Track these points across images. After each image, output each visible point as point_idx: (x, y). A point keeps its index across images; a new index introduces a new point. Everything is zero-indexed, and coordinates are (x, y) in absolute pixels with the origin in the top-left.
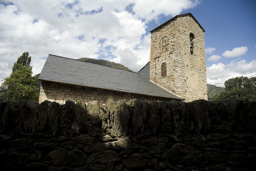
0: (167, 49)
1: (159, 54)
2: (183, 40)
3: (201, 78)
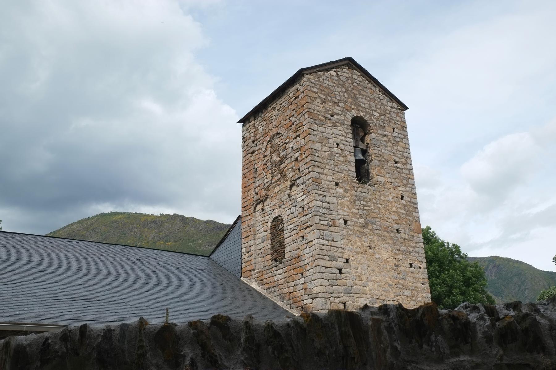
0: (282, 173)
1: (265, 189)
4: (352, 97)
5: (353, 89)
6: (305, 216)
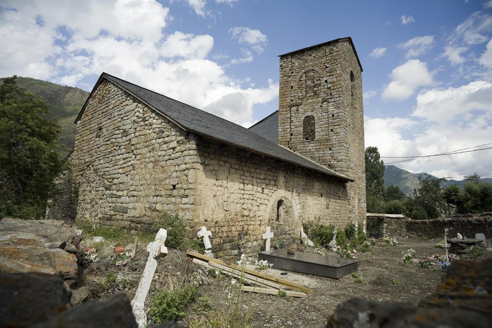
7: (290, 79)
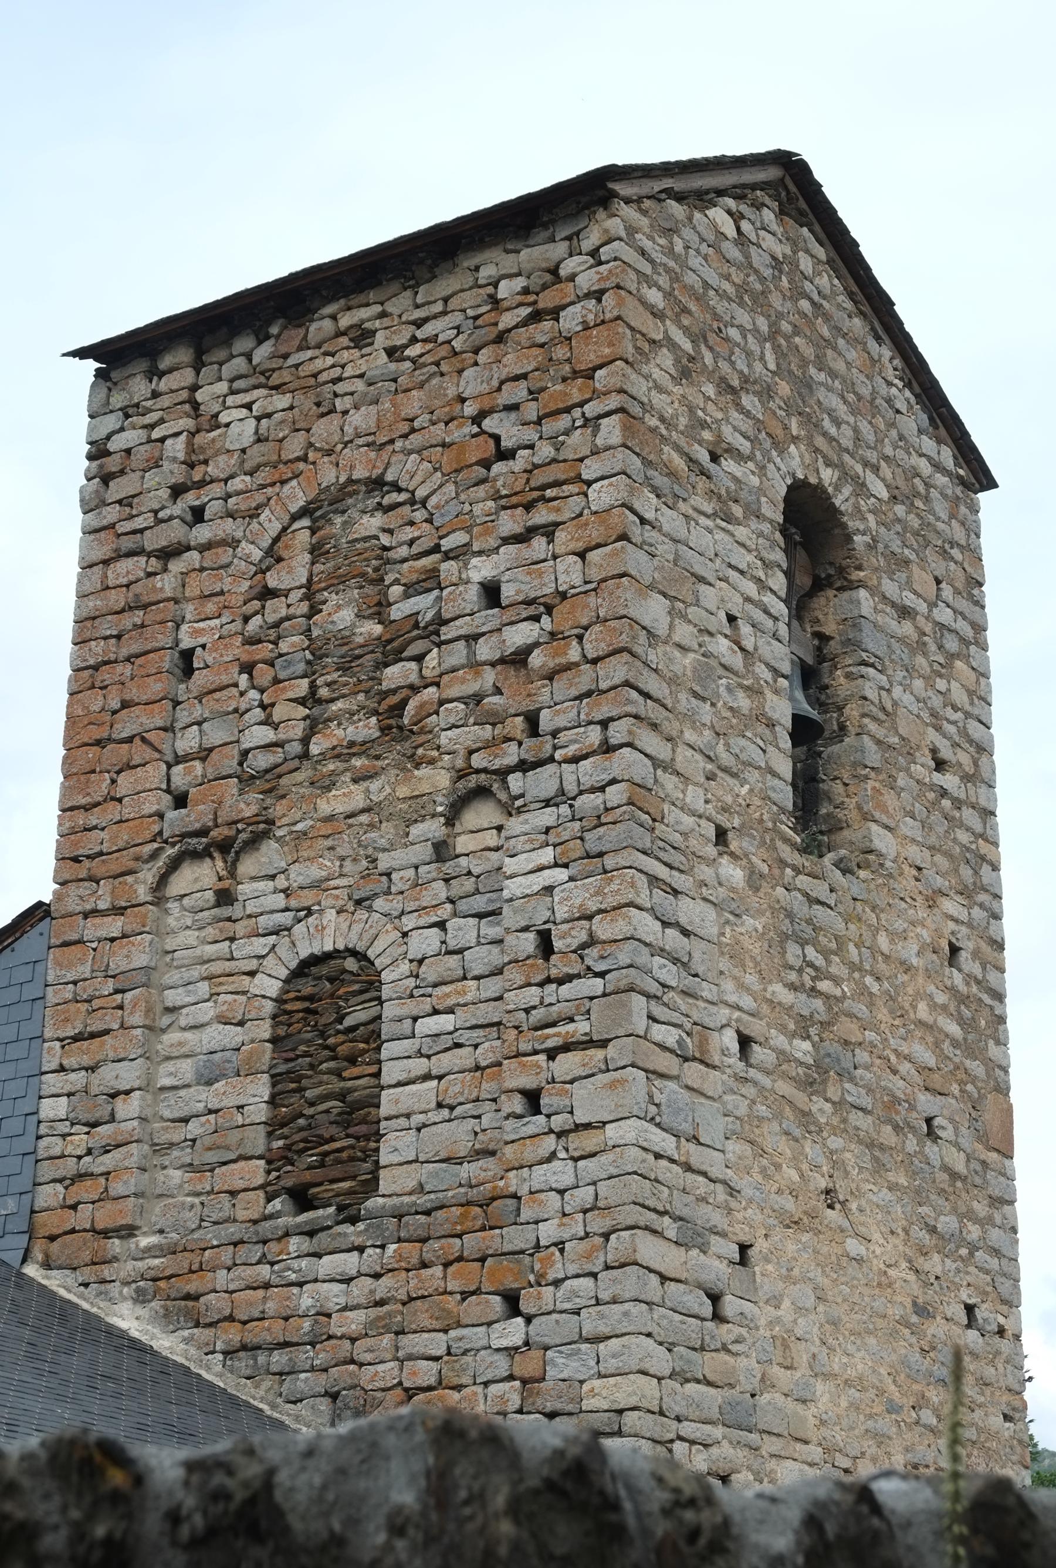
0: (394, 719)
1: (246, 781)
2: (685, 591)
3: (935, 1264)
4: (790, 372)
5: (797, 331)
6: (561, 982)
7: (166, 584)
